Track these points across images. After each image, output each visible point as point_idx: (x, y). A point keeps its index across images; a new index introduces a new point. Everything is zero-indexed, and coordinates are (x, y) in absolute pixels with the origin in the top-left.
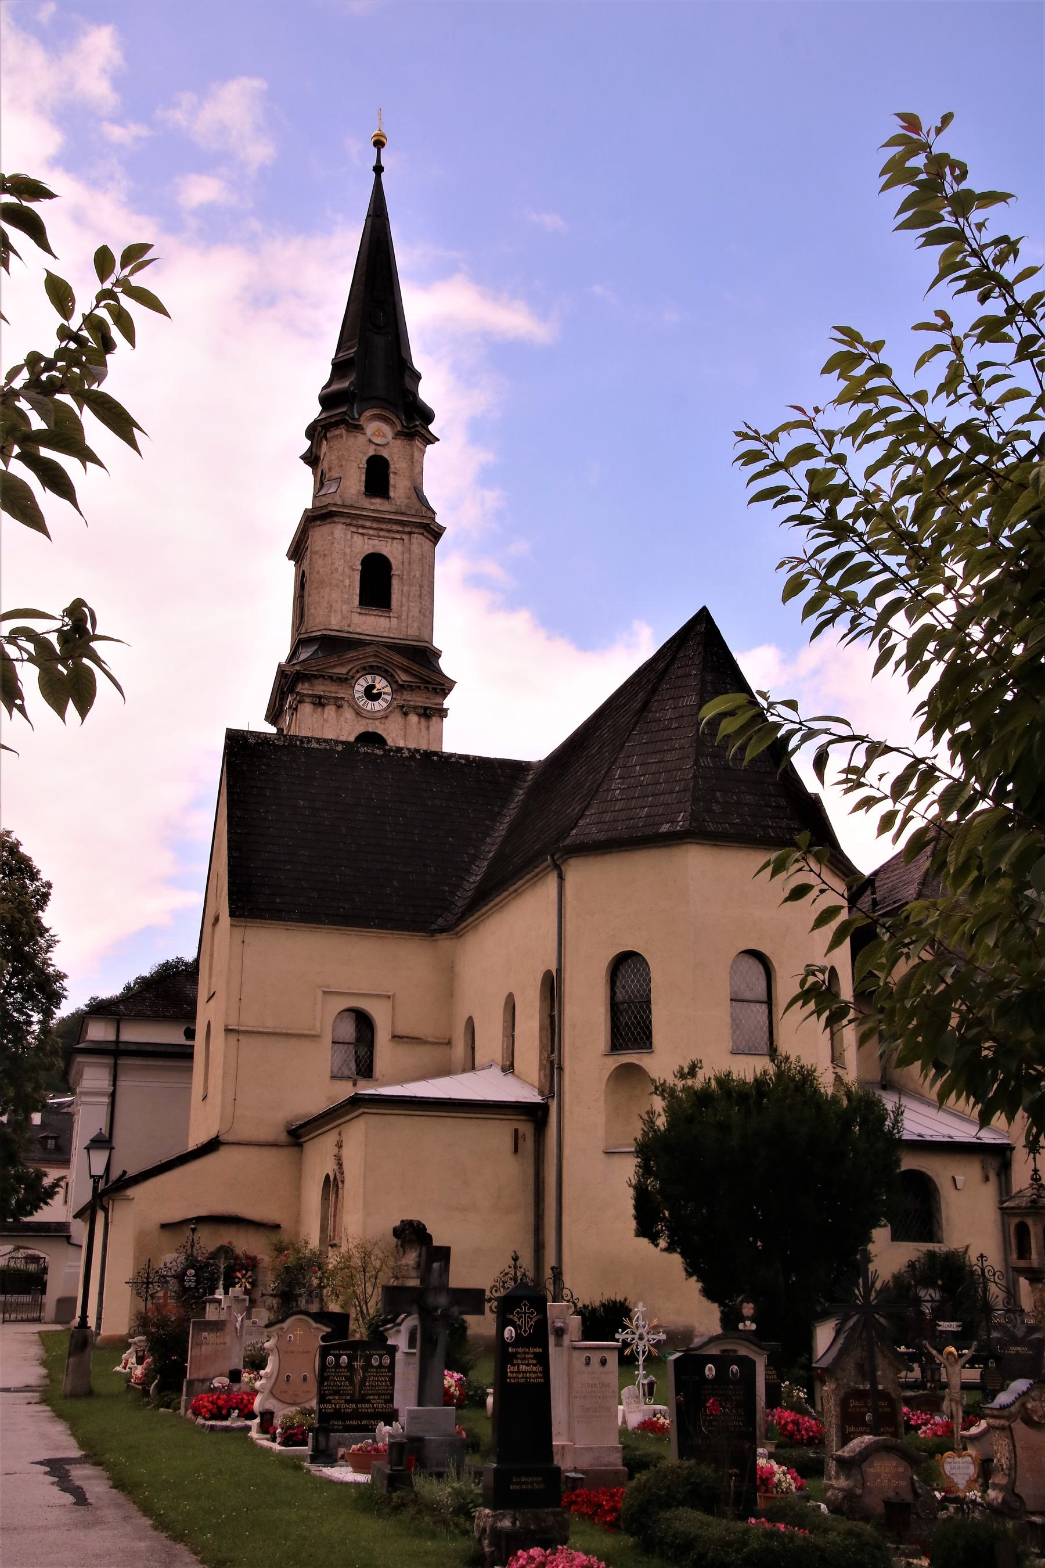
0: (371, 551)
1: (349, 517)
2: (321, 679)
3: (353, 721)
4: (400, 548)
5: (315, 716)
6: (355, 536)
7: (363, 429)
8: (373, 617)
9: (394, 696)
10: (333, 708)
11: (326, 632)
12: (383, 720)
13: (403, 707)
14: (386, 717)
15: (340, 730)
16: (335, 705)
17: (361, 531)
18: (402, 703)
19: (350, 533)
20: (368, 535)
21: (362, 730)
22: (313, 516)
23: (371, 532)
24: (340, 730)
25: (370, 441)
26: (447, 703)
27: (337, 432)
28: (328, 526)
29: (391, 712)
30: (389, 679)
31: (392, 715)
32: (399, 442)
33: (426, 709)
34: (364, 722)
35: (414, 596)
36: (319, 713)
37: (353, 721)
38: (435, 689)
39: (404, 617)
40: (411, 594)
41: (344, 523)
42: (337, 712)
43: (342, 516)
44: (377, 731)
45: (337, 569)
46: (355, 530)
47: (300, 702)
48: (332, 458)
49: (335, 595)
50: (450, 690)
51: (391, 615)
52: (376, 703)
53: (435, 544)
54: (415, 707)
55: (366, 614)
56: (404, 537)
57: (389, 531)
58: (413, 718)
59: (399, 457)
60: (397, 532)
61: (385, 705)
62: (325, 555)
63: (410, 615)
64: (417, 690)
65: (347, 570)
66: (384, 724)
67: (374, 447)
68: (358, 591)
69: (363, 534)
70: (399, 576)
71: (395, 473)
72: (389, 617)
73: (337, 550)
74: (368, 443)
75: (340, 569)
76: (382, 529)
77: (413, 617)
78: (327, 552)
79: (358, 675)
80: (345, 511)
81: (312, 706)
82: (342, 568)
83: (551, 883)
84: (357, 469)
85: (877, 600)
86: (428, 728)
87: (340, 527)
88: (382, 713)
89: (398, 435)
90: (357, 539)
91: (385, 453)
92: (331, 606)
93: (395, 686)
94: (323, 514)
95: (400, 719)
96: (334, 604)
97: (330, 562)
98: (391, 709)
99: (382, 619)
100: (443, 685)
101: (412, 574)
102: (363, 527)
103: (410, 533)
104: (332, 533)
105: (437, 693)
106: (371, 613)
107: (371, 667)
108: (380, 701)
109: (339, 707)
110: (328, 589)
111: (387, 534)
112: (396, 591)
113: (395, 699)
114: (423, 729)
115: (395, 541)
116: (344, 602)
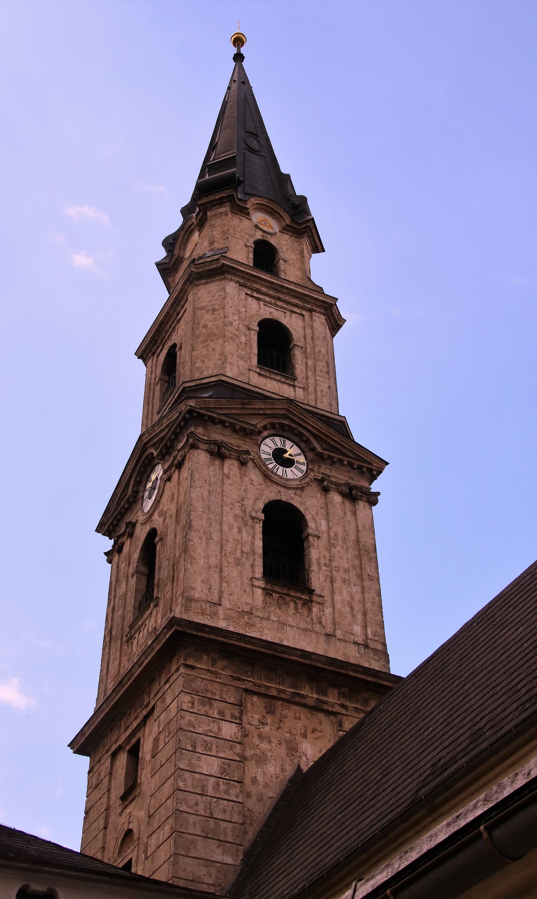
0: (268, 316)
1: (243, 277)
2: (219, 427)
3: (261, 484)
4: (300, 323)
5: (212, 468)
6: (250, 299)
7: (248, 214)
8: (275, 382)
9: (310, 467)
10: (236, 463)
11: (223, 378)
12: (298, 492)
13: (322, 481)
14: (302, 489)
15: (245, 491)
16: (238, 460)
17: (255, 295)
18: (320, 476)
19: (244, 294)
20: (264, 301)
21: (273, 496)
22: (198, 273)
23: (267, 299)
24: (245, 491)
25: (256, 226)
26: (375, 487)
27: (222, 210)
28: (218, 283)
29: (308, 483)
30: (303, 445)
31: (309, 488)
32: (286, 237)
33: (351, 488)
34: (275, 488)
35: (322, 371)
36: (217, 467)
37: (261, 484)
38: (360, 468)
39: (311, 389)
40: (318, 368)
41: (237, 282)
42: (240, 469)
43: (235, 275)
44: (292, 502)
45: (231, 324)
46: (249, 292)
47: (193, 447)
48: (214, 233)
49: (230, 347)
50: (379, 473)
51: (296, 383)
52: (288, 470)
53: (333, 336)
54: (337, 485)
55: (266, 377)
56: (304, 313)
57: (288, 303)
58: (337, 498)
59: (287, 249)
60: (296, 306)
61: (300, 475)
62: (214, 310)
63: (318, 388)
64: (337, 465)
65: (243, 329)
66: (300, 496)
67: (260, 233)
68: (255, 351)
69: (258, 299)
70: (302, 348)
71: (285, 261)
72: (294, 386)
73: (231, 305)
74: (254, 228)
75: (235, 323)
76: (279, 299)
77: (322, 391)
78: (216, 307)
79: (266, 433)
80: (240, 268)
81: (208, 455)
82: (237, 323)
83: (151, 877)
84: (244, 247)
85: (404, 675)
86: (354, 513)
87: (233, 284)
88: (296, 483)
89: (285, 229)
90: (252, 303)
91: (273, 241)
92: (226, 358)
93: (310, 455)
94: (212, 270)
95: (319, 495)
96: (229, 356)
97: (222, 315)
98: (307, 480)
99: (286, 386)
100: (372, 464)
101: (317, 349)
102: (259, 291)
103: (311, 311)
104: (224, 289)
105: (362, 473)
106: (272, 376)
107: (282, 426)
108: (293, 468)
109: (243, 464)
110: (221, 341)
111: (284, 305)
112: (299, 362)
113: (312, 470)
114: (349, 514)
115: (294, 315)
116: (241, 357)
